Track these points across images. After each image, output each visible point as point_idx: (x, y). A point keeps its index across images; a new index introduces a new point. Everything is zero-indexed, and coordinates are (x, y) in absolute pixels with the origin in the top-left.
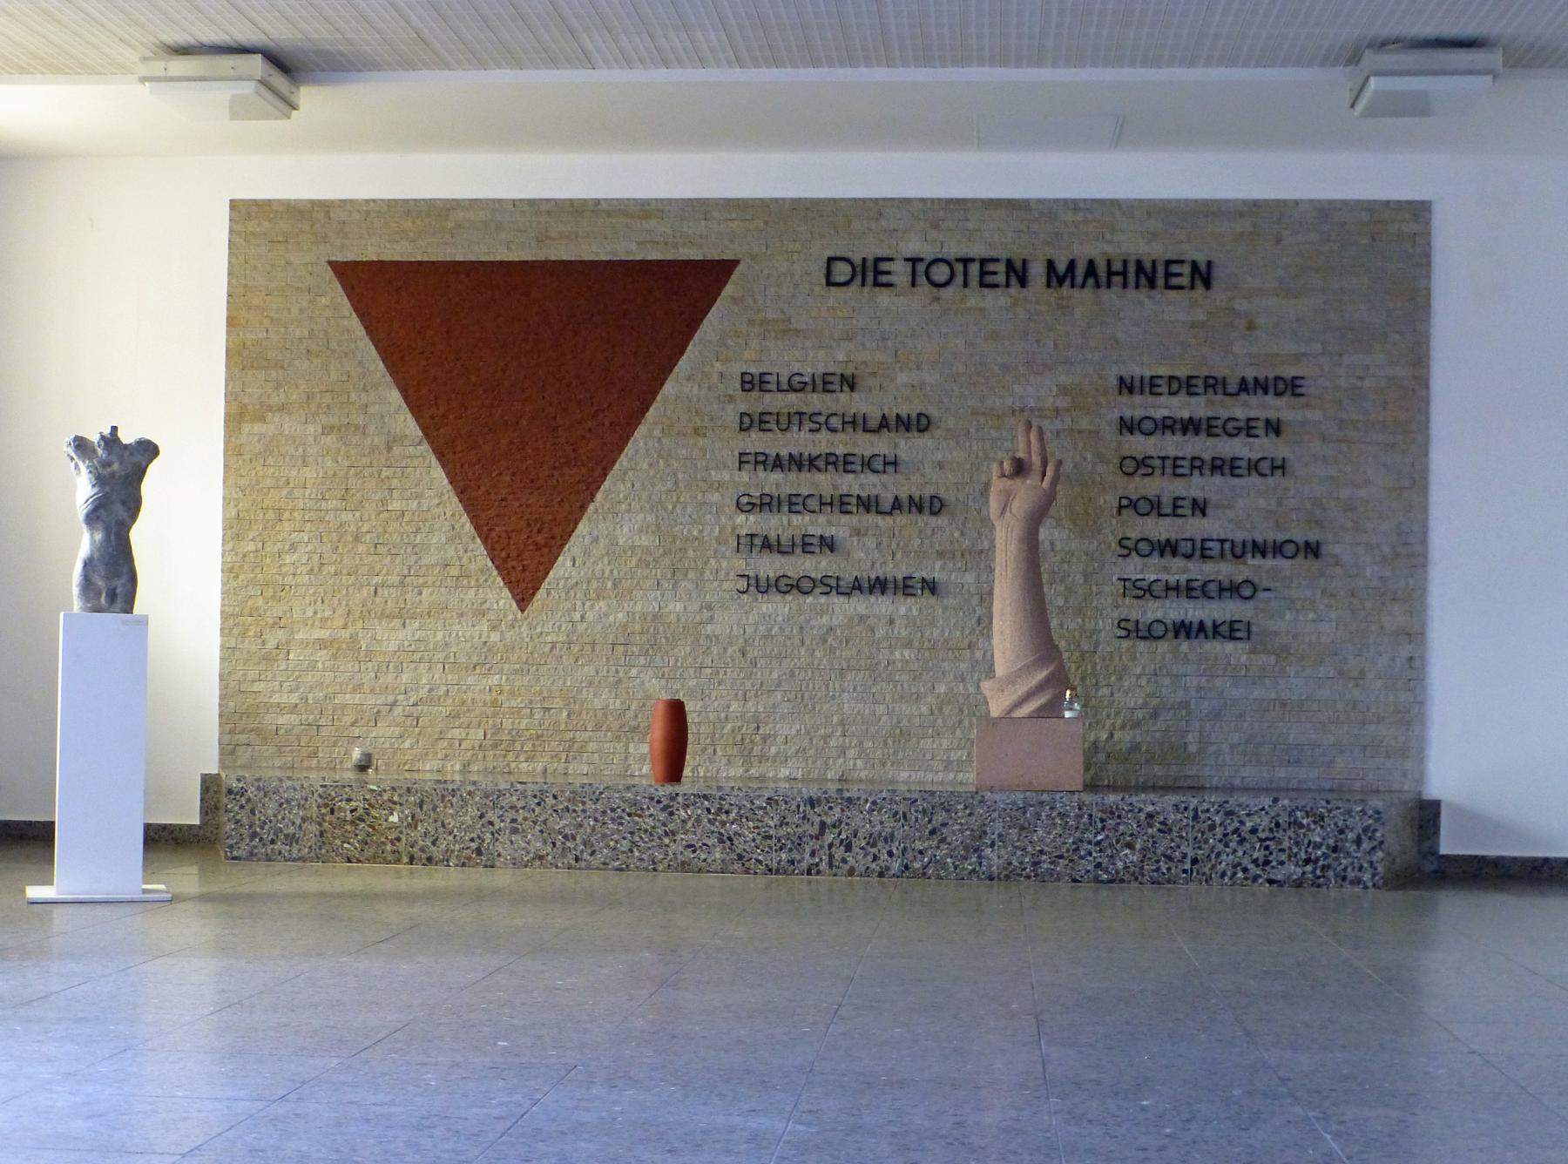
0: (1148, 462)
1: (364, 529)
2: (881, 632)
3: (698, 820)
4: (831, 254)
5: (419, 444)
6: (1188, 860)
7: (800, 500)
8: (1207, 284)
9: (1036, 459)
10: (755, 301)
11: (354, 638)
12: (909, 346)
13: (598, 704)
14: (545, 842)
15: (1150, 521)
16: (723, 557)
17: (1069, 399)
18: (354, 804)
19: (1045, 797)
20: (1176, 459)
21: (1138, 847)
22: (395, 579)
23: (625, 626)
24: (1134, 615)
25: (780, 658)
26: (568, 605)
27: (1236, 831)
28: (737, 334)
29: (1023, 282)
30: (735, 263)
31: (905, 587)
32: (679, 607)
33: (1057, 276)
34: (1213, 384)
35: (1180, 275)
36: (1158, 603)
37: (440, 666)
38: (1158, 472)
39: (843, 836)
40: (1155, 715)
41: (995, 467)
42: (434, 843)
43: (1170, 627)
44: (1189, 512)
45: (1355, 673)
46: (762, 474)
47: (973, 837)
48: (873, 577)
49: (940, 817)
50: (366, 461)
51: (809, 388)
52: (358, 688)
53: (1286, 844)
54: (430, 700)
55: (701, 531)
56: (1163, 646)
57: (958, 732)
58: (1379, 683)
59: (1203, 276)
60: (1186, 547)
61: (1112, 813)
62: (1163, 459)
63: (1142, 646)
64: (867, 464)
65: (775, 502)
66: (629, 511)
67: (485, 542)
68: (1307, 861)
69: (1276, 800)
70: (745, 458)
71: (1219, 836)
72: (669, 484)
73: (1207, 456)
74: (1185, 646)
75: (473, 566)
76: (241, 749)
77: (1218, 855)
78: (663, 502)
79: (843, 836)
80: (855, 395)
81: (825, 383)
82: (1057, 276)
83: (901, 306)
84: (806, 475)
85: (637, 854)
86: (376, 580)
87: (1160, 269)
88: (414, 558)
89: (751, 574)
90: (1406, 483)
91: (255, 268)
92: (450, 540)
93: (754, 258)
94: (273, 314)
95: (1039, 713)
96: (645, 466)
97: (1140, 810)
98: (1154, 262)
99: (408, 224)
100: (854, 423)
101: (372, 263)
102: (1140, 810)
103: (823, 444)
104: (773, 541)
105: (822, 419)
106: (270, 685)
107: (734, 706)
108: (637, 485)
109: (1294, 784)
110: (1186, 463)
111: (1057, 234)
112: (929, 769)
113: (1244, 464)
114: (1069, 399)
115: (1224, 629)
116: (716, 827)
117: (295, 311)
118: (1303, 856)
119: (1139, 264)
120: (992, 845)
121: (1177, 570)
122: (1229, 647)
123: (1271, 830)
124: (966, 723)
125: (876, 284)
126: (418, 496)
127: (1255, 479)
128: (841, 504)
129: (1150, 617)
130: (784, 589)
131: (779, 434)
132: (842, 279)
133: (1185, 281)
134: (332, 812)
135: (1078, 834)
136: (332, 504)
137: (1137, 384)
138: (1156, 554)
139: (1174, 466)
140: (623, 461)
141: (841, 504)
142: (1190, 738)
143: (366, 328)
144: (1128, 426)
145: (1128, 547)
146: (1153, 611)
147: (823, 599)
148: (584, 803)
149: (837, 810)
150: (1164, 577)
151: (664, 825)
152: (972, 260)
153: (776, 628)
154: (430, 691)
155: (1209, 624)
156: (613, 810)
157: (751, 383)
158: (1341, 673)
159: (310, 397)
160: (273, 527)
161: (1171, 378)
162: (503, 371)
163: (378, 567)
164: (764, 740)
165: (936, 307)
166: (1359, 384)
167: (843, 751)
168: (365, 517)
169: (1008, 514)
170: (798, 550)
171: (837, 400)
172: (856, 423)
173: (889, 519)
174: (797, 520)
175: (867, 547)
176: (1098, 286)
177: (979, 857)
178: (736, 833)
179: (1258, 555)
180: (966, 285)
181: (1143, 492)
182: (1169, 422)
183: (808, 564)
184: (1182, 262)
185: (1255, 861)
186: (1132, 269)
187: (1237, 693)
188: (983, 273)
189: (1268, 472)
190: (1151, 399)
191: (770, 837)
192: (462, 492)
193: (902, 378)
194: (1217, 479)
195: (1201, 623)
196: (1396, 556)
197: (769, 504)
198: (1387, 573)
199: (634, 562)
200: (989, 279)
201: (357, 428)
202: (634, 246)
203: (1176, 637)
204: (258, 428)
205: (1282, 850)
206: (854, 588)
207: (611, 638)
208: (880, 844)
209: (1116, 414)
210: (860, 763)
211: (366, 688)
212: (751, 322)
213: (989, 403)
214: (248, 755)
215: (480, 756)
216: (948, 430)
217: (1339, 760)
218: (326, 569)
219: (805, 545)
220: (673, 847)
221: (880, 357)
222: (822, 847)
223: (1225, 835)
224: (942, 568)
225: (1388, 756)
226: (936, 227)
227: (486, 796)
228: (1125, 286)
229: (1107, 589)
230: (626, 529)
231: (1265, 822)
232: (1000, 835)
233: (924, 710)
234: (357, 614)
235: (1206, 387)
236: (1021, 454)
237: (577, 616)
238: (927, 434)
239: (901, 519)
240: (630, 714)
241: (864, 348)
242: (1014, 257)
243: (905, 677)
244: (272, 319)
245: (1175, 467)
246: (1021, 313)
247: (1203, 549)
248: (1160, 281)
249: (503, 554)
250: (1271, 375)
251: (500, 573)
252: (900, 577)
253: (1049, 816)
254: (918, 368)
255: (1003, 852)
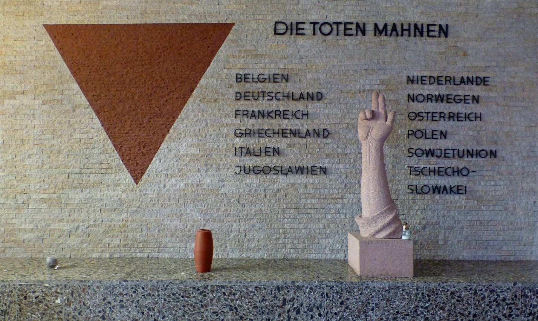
0: (420, 114)
1: (63, 148)
2: (301, 191)
3: (219, 299)
4: (277, 20)
5: (88, 108)
6: (471, 315)
7: (264, 132)
8: (446, 35)
9: (381, 110)
10: (242, 41)
11: (59, 198)
12: (313, 62)
13: (172, 225)
14: (138, 312)
15: (421, 141)
16: (229, 158)
17: (384, 86)
18: (37, 294)
19: (399, 285)
20: (433, 113)
21: (447, 309)
22: (77, 170)
23: (184, 190)
24: (415, 183)
25: (256, 203)
26: (158, 180)
27: (495, 300)
28: (234, 56)
29: (364, 33)
30: (233, 24)
31: (312, 171)
32: (209, 180)
33: (379, 31)
34: (449, 80)
35: (434, 31)
36: (425, 177)
37: (99, 210)
38: (425, 119)
39: (295, 306)
40: (424, 228)
41: (361, 115)
42: (79, 314)
43: (431, 188)
44: (439, 137)
45: (512, 209)
46: (246, 120)
47: (363, 306)
48: (297, 166)
49: (345, 295)
50: (63, 116)
51: (267, 80)
52: (61, 221)
53: (520, 306)
54: (95, 225)
55: (218, 146)
56: (427, 197)
57: (337, 236)
58: (521, 213)
59: (444, 31)
60: (438, 153)
61: (434, 292)
62: (428, 113)
63: (418, 197)
64: (294, 115)
65: (252, 132)
66: (185, 137)
67: (119, 152)
68: (530, 314)
69: (515, 284)
70: (238, 113)
71: (487, 303)
72: (203, 125)
73: (446, 112)
74: (437, 197)
75: (113, 164)
76: (7, 250)
77: (486, 312)
78: (199, 136)
79: (295, 306)
80: (288, 84)
81: (274, 78)
82: (379, 31)
83: (308, 43)
84: (266, 120)
85: (187, 317)
86: (69, 171)
87: (425, 29)
88: (86, 160)
89: (242, 165)
90: (533, 125)
91: (9, 28)
92: (103, 152)
93: (241, 22)
94: (17, 49)
95: (389, 236)
96: (192, 116)
97: (448, 290)
98: (422, 25)
99: (80, 7)
100: (288, 96)
101: (64, 25)
102: (448, 290)
103: (274, 106)
104: (252, 150)
105: (273, 95)
106: (20, 220)
107: (235, 226)
108: (189, 125)
109: (485, 258)
110: (437, 115)
111: (378, 12)
112: (324, 253)
113: (463, 115)
114: (384, 86)
115: (455, 189)
116: (229, 303)
117: (28, 47)
118: (528, 311)
119: (416, 26)
120: (373, 309)
121: (433, 163)
122: (457, 197)
123: (513, 299)
124: (340, 232)
125: (297, 34)
126: (88, 132)
127: (468, 122)
128: (283, 133)
129: (422, 184)
130: (257, 172)
131: (254, 102)
132: (282, 32)
133: (436, 34)
134: (25, 298)
135: (416, 303)
136: (47, 136)
137: (415, 79)
138: (425, 155)
139: (432, 116)
140: (182, 115)
141: (283, 133)
142: (440, 238)
143: (62, 55)
144: (411, 98)
145: (412, 153)
146: (423, 181)
147: (275, 176)
148: (158, 291)
149: (292, 292)
150: (428, 166)
151: (201, 302)
152: (341, 23)
153: (253, 190)
154: (95, 221)
155: (448, 187)
156: (174, 294)
157: (240, 79)
158: (506, 209)
159: (36, 88)
160: (20, 147)
161: (430, 77)
162: (126, 74)
163: (69, 165)
164: (249, 241)
165: (324, 44)
166: (512, 80)
167: (285, 245)
168: (63, 142)
169: (369, 137)
170: (263, 154)
171: (280, 86)
172: (288, 96)
173: (304, 140)
174: (262, 140)
175: (295, 153)
176: (397, 35)
177: (366, 316)
178: (239, 305)
179: (470, 156)
180: (338, 34)
181: (418, 128)
182: (430, 97)
183: (268, 160)
184: (435, 25)
185: (504, 315)
186: (412, 28)
187: (461, 218)
188: (346, 29)
189: (474, 119)
190: (421, 86)
191: (257, 307)
192: (107, 130)
193: (309, 76)
194: (451, 122)
195: (445, 187)
196: (529, 156)
197: (250, 133)
198: (525, 164)
199: (188, 161)
200: (348, 32)
201: (58, 101)
202: (186, 17)
203: (434, 192)
204: (12, 102)
205: (518, 309)
206: (289, 171)
207: (178, 195)
208: (315, 310)
209: (406, 93)
210: (292, 251)
211: (65, 221)
212: (240, 51)
213: (349, 87)
214: (11, 252)
215: (119, 250)
216: (331, 100)
217: (505, 247)
218: (45, 166)
219: (266, 152)
220: (206, 313)
221: (299, 67)
222: (284, 312)
223: (490, 302)
224: (329, 162)
225: (525, 245)
226: (324, 8)
227: (107, 288)
228: (409, 35)
229: (403, 171)
230: (184, 146)
231: (509, 295)
232: (377, 304)
233: (321, 226)
234: (60, 187)
235: (446, 81)
236: (373, 109)
237: (162, 186)
238: (321, 101)
239: (310, 140)
240: (187, 230)
241: (292, 63)
242: (359, 22)
243: (312, 212)
244: (17, 52)
245: (433, 117)
246: (363, 47)
247: (445, 153)
248: (425, 34)
249: (128, 158)
250: (475, 76)
251: (126, 167)
252: (310, 166)
253: (401, 294)
254: (317, 71)
255: (378, 313)
